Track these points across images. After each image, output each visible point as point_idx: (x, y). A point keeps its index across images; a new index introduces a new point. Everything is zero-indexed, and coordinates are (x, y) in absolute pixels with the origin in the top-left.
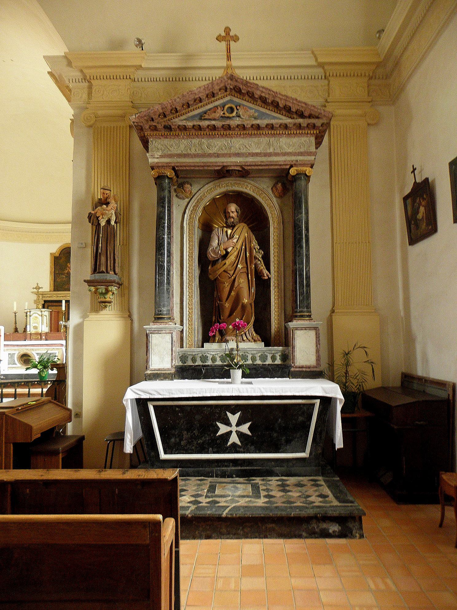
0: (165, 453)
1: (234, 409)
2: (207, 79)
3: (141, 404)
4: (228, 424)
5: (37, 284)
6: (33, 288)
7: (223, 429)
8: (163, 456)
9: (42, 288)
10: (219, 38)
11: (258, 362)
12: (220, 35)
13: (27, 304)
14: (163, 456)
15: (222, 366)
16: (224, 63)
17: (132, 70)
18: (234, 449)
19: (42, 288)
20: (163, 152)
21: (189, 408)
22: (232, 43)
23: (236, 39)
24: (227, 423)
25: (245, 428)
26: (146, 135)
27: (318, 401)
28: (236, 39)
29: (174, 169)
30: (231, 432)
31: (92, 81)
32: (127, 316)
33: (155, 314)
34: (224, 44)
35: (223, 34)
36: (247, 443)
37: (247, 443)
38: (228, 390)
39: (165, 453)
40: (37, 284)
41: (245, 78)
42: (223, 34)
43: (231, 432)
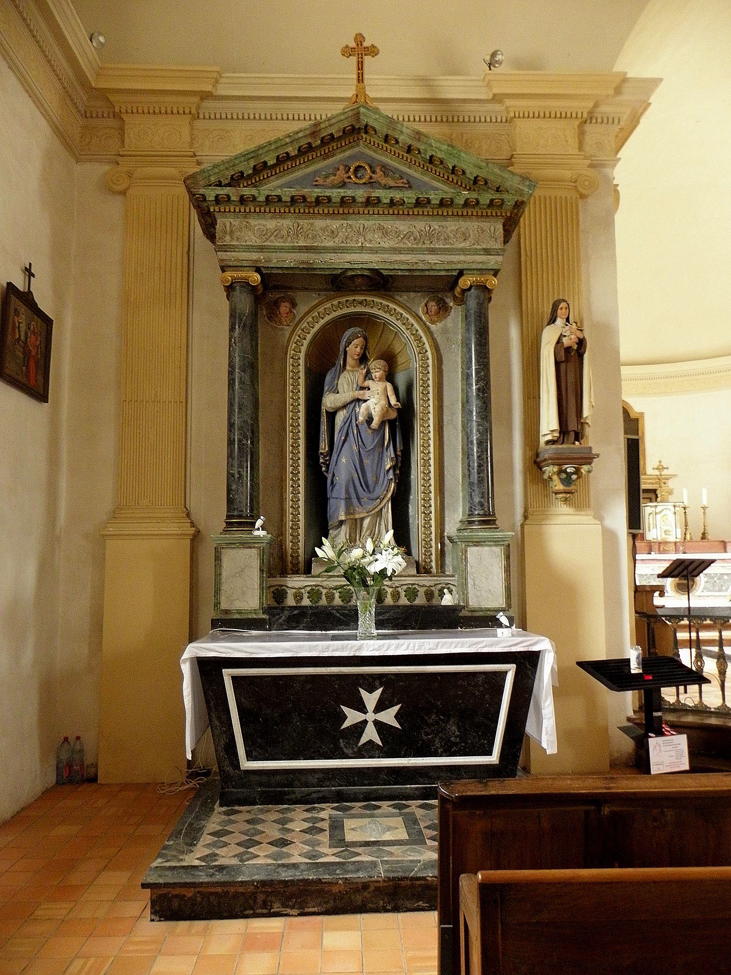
0: (489, 753)
1: (370, 683)
2: (307, 118)
3: (209, 669)
4: (379, 708)
5: (660, 462)
6: (654, 469)
7: (352, 717)
8: (494, 758)
9: (667, 468)
10: (347, 52)
11: (306, 602)
12: (347, 47)
13: (705, 492)
14: (494, 758)
15: (326, 607)
16: (350, 93)
17: (196, 99)
18: (369, 750)
19: (667, 468)
20: (265, 239)
21: (480, 680)
22: (367, 59)
23: (373, 51)
24: (361, 707)
25: (389, 717)
26: (212, 210)
27: (511, 669)
28: (373, 51)
29: (258, 270)
30: (365, 722)
31: (124, 116)
32: (184, 515)
33: (228, 517)
34: (354, 60)
35: (353, 44)
36: (393, 741)
37: (393, 741)
38: (343, 648)
39: (489, 753)
40: (660, 462)
41: (395, 117)
42: (353, 44)
43: (365, 722)
